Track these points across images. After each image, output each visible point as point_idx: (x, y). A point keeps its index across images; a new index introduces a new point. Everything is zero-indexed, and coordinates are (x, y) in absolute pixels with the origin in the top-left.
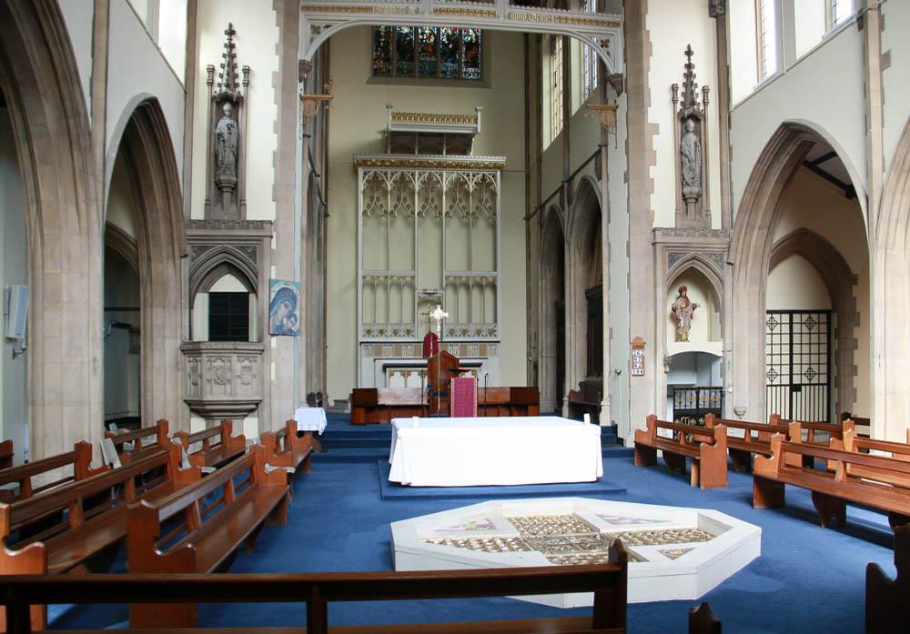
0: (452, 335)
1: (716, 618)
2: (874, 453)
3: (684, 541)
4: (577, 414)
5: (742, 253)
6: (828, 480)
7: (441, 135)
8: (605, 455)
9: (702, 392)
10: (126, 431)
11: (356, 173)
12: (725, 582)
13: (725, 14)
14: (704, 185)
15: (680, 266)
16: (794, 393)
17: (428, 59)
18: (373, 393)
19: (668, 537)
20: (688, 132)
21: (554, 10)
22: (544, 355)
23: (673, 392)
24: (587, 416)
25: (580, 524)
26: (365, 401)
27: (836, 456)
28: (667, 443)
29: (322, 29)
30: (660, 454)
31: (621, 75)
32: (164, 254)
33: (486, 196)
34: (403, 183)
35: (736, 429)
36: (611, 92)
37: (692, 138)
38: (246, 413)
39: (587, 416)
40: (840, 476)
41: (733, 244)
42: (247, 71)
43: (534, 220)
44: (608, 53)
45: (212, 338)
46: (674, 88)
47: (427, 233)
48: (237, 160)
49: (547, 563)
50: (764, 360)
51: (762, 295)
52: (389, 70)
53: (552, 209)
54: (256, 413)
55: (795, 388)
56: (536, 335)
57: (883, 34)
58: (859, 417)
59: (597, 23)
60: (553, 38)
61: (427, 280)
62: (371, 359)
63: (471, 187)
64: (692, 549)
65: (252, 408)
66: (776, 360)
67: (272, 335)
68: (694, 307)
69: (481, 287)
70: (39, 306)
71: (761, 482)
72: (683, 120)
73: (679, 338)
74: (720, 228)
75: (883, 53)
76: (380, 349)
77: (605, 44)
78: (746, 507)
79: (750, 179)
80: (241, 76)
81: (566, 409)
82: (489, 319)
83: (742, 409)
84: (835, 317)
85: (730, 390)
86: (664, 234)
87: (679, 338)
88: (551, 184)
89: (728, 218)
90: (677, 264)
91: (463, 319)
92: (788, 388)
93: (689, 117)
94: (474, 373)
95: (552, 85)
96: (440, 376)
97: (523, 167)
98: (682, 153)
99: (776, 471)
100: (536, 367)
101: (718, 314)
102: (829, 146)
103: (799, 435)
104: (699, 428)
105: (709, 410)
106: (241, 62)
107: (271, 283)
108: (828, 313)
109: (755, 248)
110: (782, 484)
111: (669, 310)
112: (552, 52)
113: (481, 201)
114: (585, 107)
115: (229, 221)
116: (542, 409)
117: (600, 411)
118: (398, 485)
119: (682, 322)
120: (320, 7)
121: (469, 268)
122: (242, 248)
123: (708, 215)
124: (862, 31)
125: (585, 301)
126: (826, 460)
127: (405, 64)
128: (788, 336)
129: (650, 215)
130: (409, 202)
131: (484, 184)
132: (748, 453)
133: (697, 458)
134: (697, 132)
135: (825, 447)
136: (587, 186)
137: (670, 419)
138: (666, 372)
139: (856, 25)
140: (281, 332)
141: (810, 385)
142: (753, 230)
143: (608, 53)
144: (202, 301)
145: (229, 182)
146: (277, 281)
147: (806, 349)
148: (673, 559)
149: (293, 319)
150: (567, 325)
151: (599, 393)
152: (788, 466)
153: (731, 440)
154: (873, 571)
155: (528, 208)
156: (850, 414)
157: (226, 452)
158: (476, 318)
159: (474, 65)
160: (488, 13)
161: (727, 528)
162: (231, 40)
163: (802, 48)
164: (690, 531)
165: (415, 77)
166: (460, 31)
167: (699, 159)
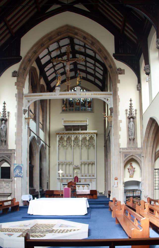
7: (79, 126)
11: (56, 136)
14: (135, 136)
17: (77, 106)
20: (131, 122)
21: (33, 93)
23: (126, 191)
29: (30, 101)
34: (69, 139)
37: (132, 123)
38: (8, 196)
42: (9, 113)
46: (126, 110)
47: (77, 151)
52: (67, 110)
54: (11, 196)
61: (77, 163)
67: (15, 177)
72: (129, 119)
76: (63, 180)
79: (145, 133)
83: (146, 196)
93: (131, 118)
98: (129, 128)
106: (7, 110)
107: (14, 164)
109: (149, 152)
115: (3, 150)
118: (30, 215)
120: (98, 94)
121: (88, 159)
122: (7, 156)
127: (71, 108)
129: (119, 145)
131: (91, 138)
140: (17, 176)
145: (4, 140)
146: (16, 164)
149: (21, 173)
162: (4, 105)
165: (73, 111)
166: (86, 99)
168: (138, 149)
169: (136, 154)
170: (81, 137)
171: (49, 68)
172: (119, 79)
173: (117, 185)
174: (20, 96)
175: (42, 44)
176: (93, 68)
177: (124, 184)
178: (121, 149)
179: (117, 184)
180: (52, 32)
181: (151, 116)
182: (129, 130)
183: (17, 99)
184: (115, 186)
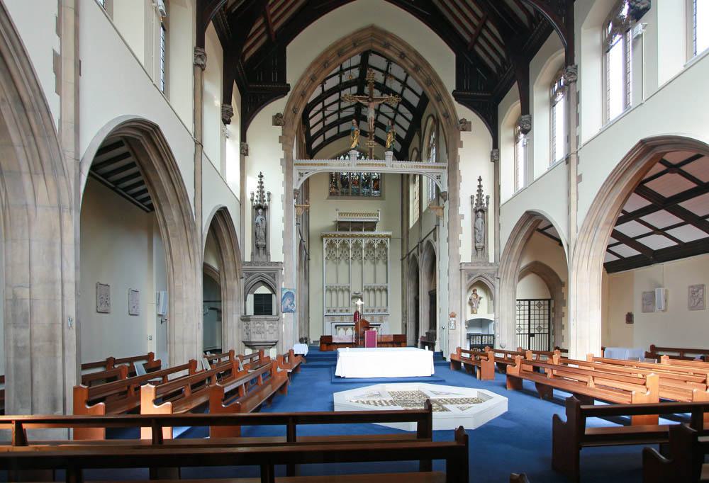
2: (570, 365)
6: (544, 378)
7: (362, 222)
8: (435, 365)
9: (484, 337)
10: (214, 355)
12: (488, 422)
15: (473, 280)
18: (330, 337)
23: (470, 337)
24: (427, 347)
26: (327, 341)
30: (462, 364)
31: (446, 192)
32: (232, 277)
33: (383, 250)
34: (344, 245)
36: (441, 200)
37: (480, 220)
39: (427, 347)
40: (549, 375)
42: (269, 194)
43: (405, 260)
45: (255, 314)
46: (472, 197)
47: (355, 266)
48: (265, 235)
53: (414, 255)
55: (531, 335)
56: (406, 312)
57: (579, 166)
59: (435, 167)
60: (415, 175)
61: (355, 288)
62: (330, 323)
63: (376, 246)
65: (274, 344)
68: (480, 298)
69: (380, 290)
70: (172, 300)
73: (473, 312)
77: (438, 177)
78: (502, 389)
80: (266, 196)
81: (419, 344)
82: (384, 304)
84: (552, 302)
87: (473, 312)
88: (413, 243)
90: (470, 280)
91: (372, 305)
93: (479, 211)
94: (377, 328)
96: (361, 330)
99: (518, 373)
100: (406, 326)
105: (488, 345)
106: (266, 190)
108: (549, 300)
110: (521, 379)
112: (414, 182)
116: (408, 344)
121: (375, 282)
123: (488, 256)
125: (429, 297)
127: (344, 190)
129: (459, 257)
130: (347, 253)
134: (483, 218)
135: (545, 363)
136: (429, 243)
137: (468, 349)
139: (565, 162)
140: (287, 311)
144: (251, 298)
147: (537, 317)
153: (496, 359)
154: (556, 418)
155: (402, 254)
157: (260, 362)
158: (378, 304)
159: (377, 189)
160: (383, 165)
161: (491, 398)
163: (537, 175)
168: (491, 264)
170: (364, 243)
171: (316, 112)
172: (461, 140)
174: (287, 165)
175: (326, 62)
176: (392, 115)
180: (344, 39)
183: (285, 170)
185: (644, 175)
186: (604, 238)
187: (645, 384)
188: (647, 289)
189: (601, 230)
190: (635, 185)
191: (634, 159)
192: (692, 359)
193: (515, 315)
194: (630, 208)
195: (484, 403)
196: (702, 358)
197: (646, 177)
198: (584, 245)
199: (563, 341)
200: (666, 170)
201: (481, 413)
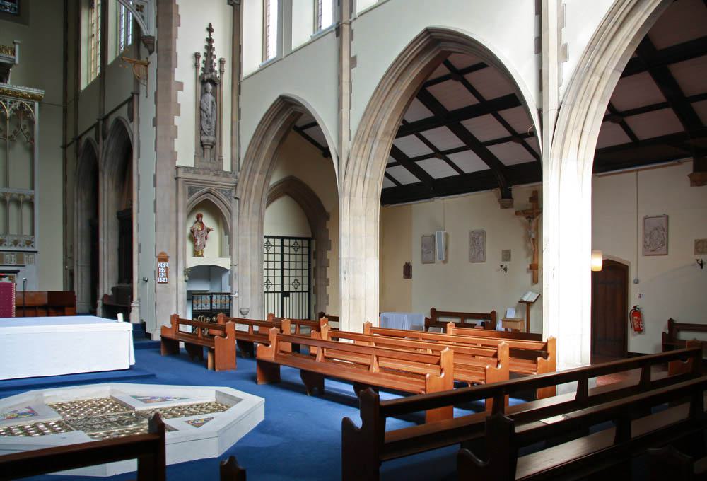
0: (28, 246)
1: (241, 467)
3: (206, 413)
4: (110, 313)
5: (246, 192)
8: (136, 347)
9: (214, 297)
12: (240, 441)
13: (239, 4)
15: (197, 198)
16: (285, 298)
19: (192, 410)
20: (207, 92)
22: (79, 264)
23: (191, 296)
24: (120, 316)
25: (116, 403)
27: (316, 343)
28: (186, 336)
30: (182, 345)
31: (153, 37)
35: (241, 325)
36: (144, 51)
39: (120, 316)
40: (319, 358)
41: (240, 184)
43: (71, 149)
44: (143, 17)
46: (197, 56)
49: (90, 440)
50: (262, 273)
51: (261, 223)
53: (88, 141)
55: (285, 294)
56: (72, 247)
57: (139, 160)
58: (330, 315)
64: (213, 418)
66: (271, 273)
68: (209, 230)
71: (263, 364)
73: (196, 254)
74: (230, 171)
75: (352, 56)
78: (251, 384)
81: (99, 310)
82: (27, 231)
84: (314, 243)
85: (237, 295)
86: (185, 172)
87: (196, 254)
88: (88, 119)
89: (236, 164)
92: (280, 294)
93: (208, 81)
94: (12, 278)
95: (90, 35)
97: (60, 101)
98: (201, 109)
99: (273, 356)
100: (72, 274)
101: (227, 236)
102: (313, 118)
103: (289, 329)
104: (213, 324)
105: (221, 310)
108: (309, 240)
110: (278, 365)
111: (188, 231)
113: (18, 126)
114: (120, 59)
116: (78, 311)
117: (130, 311)
119: (198, 242)
123: (221, 159)
124: (339, 38)
125: (117, 221)
126: (309, 346)
128: (280, 255)
129: (174, 156)
131: (22, 112)
132: (252, 343)
133: (213, 348)
135: (308, 337)
136: (119, 124)
137: (189, 317)
138: (186, 281)
141: (296, 292)
142: (255, 173)
143: (143, 17)
145: (208, 141)
147: (293, 265)
148: (198, 426)
150: (101, 240)
151: (130, 296)
152: (282, 352)
153: (239, 333)
154: (347, 423)
156: (324, 314)
158: (13, 229)
161: (239, 400)
163: (295, 45)
164: (209, 404)
167: (214, 115)
169: (218, 190)
173: (167, 276)
177: (189, 275)
178: (179, 169)
179: (167, 273)
181: (289, 91)
182: (201, 116)
184: (160, 280)
185: (428, 76)
186: (381, 156)
187: (439, 363)
188: (428, 232)
189: (380, 141)
190: (417, 89)
191: (417, 52)
192: (472, 326)
193: (262, 261)
194: (411, 119)
195: (229, 410)
196: (483, 324)
197: (433, 77)
198: (359, 159)
199: (328, 304)
200: (449, 75)
201: (229, 427)
